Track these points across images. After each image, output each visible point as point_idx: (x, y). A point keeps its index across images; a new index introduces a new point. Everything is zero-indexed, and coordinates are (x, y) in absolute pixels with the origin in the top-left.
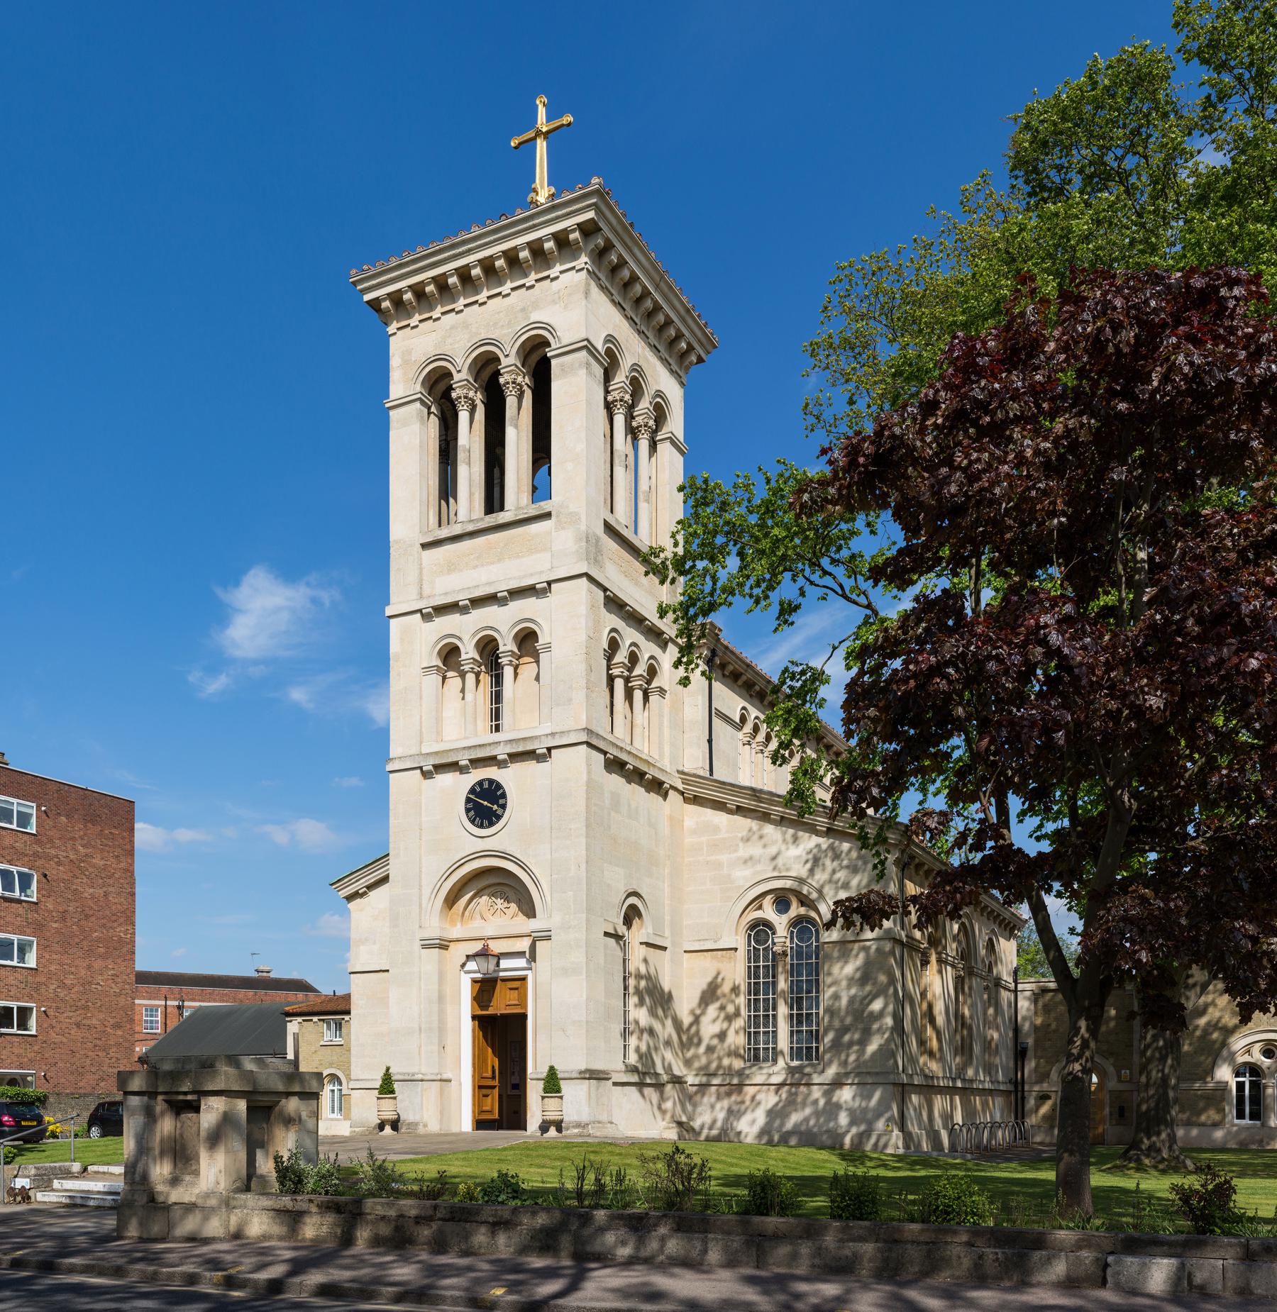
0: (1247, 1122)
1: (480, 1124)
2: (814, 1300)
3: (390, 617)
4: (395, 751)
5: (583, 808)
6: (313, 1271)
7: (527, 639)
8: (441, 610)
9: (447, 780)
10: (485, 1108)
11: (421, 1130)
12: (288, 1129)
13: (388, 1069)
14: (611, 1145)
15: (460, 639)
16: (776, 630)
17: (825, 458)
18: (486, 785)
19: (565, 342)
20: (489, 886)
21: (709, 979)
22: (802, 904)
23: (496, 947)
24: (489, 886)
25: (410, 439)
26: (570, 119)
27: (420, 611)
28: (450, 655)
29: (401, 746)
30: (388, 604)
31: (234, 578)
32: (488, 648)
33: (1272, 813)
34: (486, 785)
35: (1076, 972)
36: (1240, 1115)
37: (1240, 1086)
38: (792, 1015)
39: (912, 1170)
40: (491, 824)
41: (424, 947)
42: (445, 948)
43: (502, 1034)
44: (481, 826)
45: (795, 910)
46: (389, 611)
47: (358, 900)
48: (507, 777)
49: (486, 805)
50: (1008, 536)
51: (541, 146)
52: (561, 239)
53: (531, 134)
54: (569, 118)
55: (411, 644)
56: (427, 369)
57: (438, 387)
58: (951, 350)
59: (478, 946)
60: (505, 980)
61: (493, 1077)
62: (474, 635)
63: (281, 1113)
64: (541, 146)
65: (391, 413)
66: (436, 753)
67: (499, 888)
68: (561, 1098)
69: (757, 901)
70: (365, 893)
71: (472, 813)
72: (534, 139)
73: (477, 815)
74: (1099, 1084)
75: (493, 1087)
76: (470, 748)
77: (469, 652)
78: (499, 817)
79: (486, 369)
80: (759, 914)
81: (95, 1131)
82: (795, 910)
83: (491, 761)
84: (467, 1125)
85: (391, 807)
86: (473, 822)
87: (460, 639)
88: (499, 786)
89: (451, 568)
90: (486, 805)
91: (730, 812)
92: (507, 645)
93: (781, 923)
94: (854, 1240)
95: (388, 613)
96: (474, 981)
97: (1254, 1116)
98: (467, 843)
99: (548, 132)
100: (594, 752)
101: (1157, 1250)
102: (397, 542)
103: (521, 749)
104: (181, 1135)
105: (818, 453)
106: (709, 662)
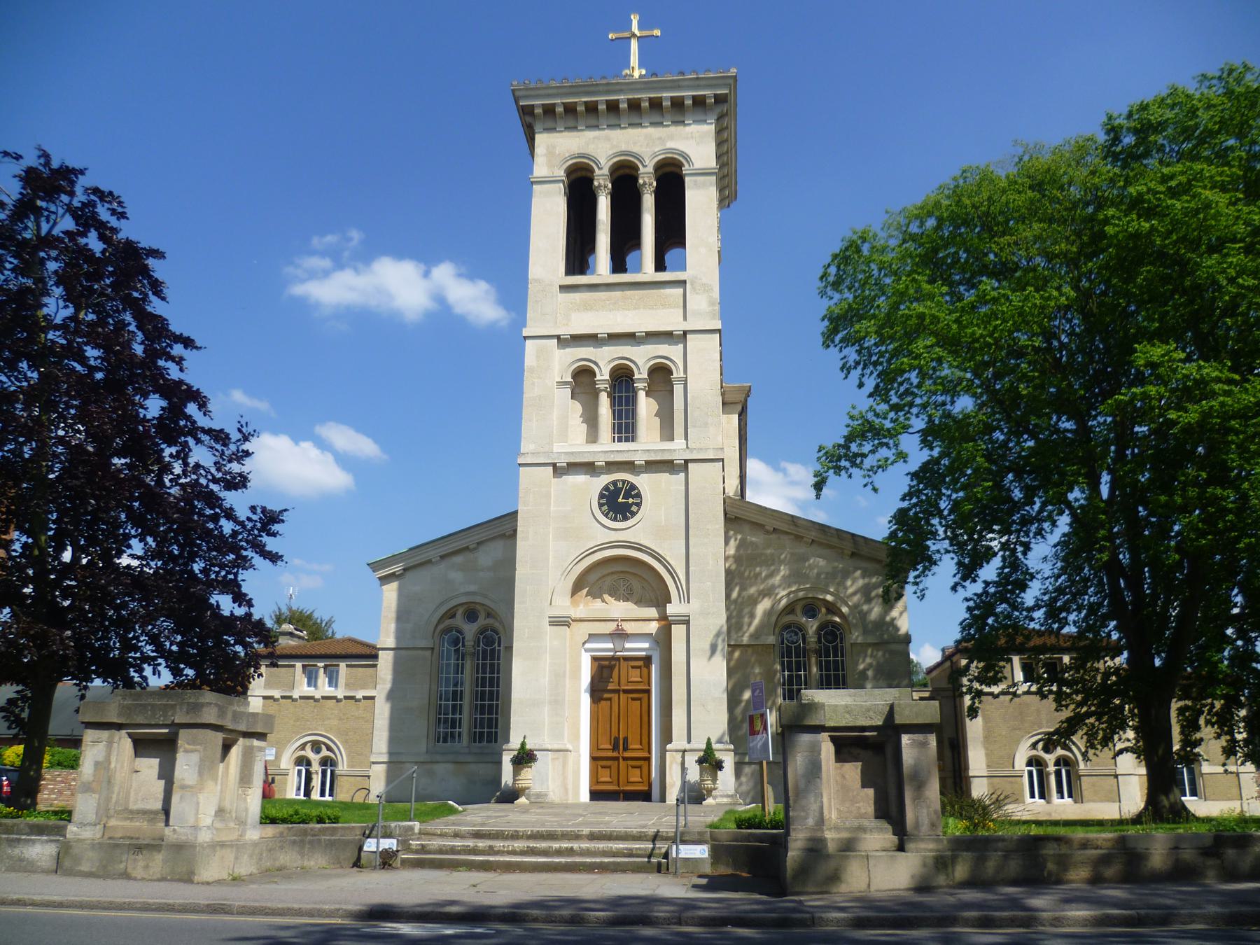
0: (1067, 800)
1: (596, 795)
3: (525, 338)
4: (524, 448)
6: (332, 424)
7: (661, 375)
8: (578, 340)
9: (581, 479)
10: (632, 779)
12: (894, 834)
13: (818, 497)
14: (1046, 159)
16: (15, 176)
18: (603, 501)
19: (696, 166)
22: (453, 616)
23: (629, 628)
25: (549, 215)
27: (558, 337)
28: (583, 377)
29: (529, 446)
32: (622, 378)
33: (4, 494)
35: (161, 363)
36: (1033, 796)
37: (1030, 773)
39: (801, 902)
40: (625, 519)
41: (552, 624)
45: (482, 621)
48: (643, 482)
49: (619, 503)
51: (634, 45)
52: (699, 102)
54: (657, 32)
57: (579, 187)
58: (977, 340)
59: (610, 628)
60: (626, 659)
62: (610, 362)
63: (201, 845)
64: (634, 45)
65: (751, 497)
66: (572, 453)
67: (622, 576)
68: (375, 666)
69: (451, 614)
70: (475, 549)
73: (610, 509)
76: (454, 866)
77: (603, 375)
78: (633, 514)
79: (625, 180)
80: (303, 753)
81: (268, 590)
83: (629, 466)
84: (585, 796)
86: (601, 505)
88: (601, 496)
89: (587, 307)
90: (619, 503)
91: (768, 532)
92: (641, 374)
93: (470, 630)
94: (334, 698)
95: (525, 334)
96: (594, 659)
97: (1042, 796)
98: (601, 534)
100: (195, 731)
101: (504, 914)
105: (814, 493)
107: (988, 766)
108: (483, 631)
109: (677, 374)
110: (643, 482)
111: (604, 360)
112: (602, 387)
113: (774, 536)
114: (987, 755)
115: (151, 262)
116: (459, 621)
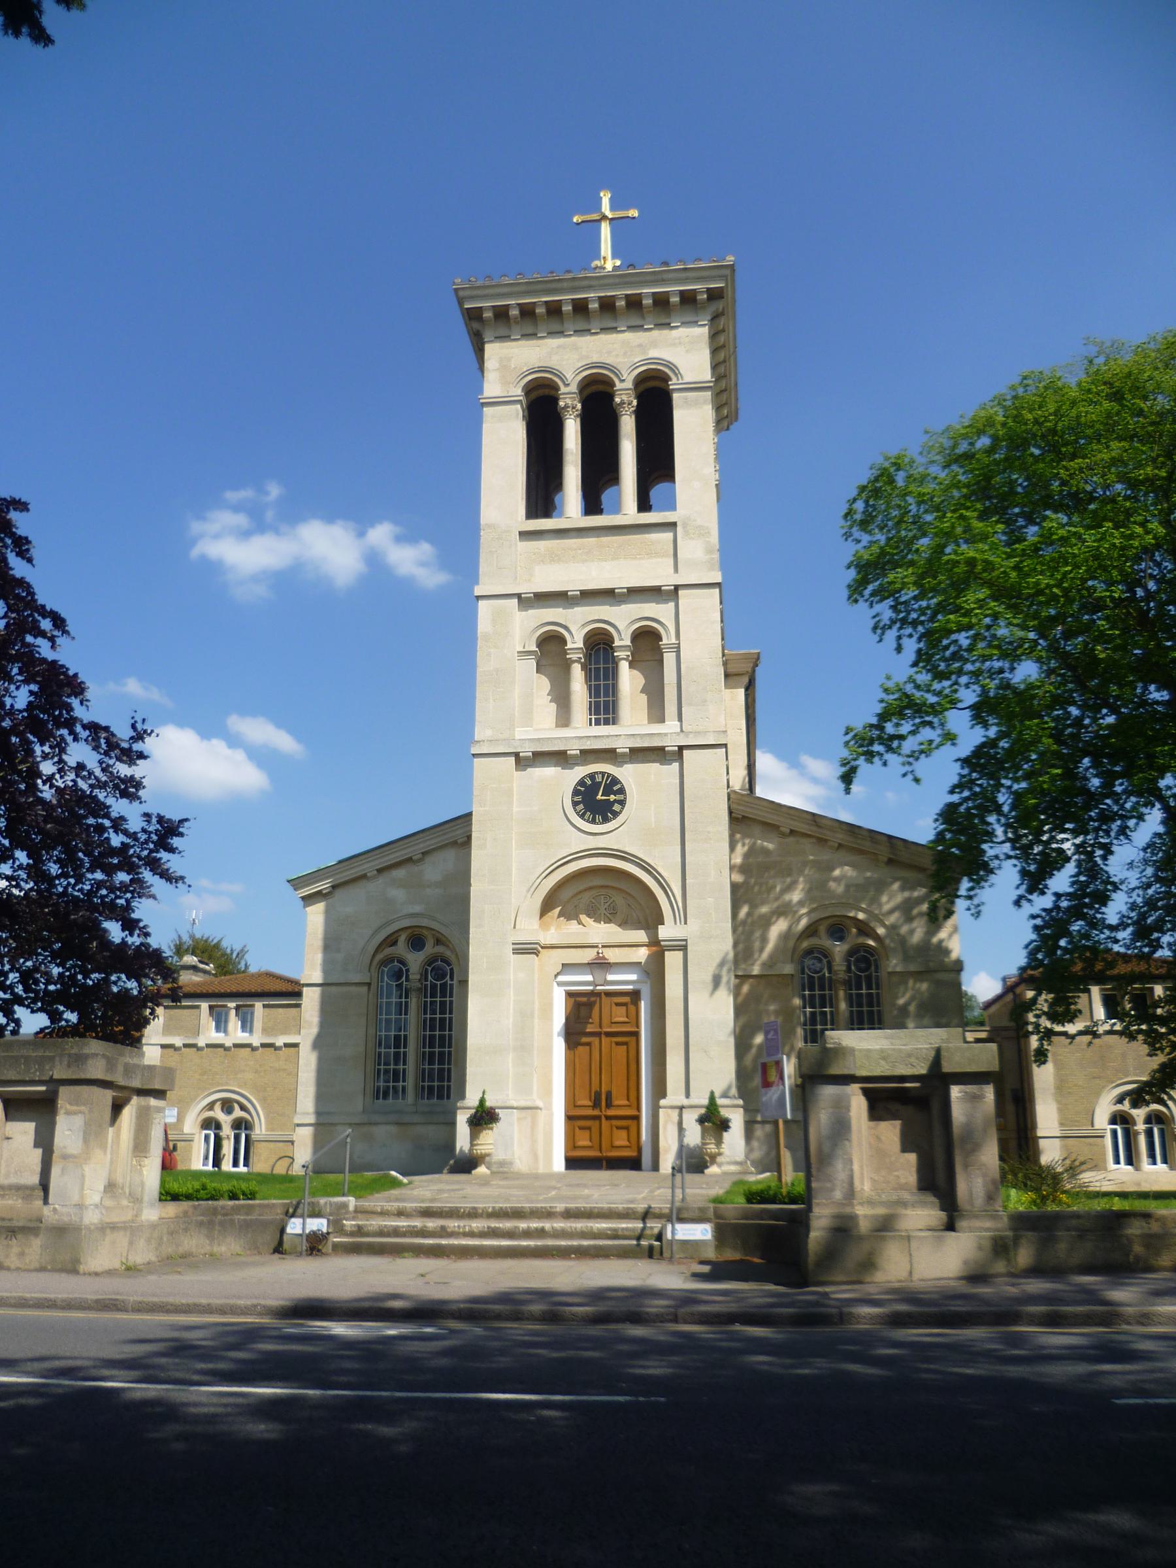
1: (573, 1163)
2: (756, 956)
5: (190, 1203)
7: (647, 640)
9: (549, 772)
11: (398, 530)
15: (566, 628)
17: (850, 539)
20: (591, 888)
21: (724, 792)
22: (395, 943)
23: (612, 956)
24: (591, 888)
25: (504, 443)
26: (636, 214)
28: (550, 645)
30: (477, 583)
31: (431, 541)
32: (599, 645)
34: (577, 799)
37: (1114, 1132)
38: (878, 1005)
40: (606, 820)
41: (517, 952)
42: (536, 953)
43: (541, 757)
44: (593, 822)
45: (430, 949)
46: (478, 591)
47: (655, 766)
48: (627, 774)
49: (598, 801)
50: (80, 977)
51: (605, 230)
52: (688, 299)
53: (595, 216)
54: (634, 213)
55: (505, 637)
56: (594, 371)
59: (588, 956)
60: (609, 994)
61: (589, 1128)
62: (633, 622)
64: (605, 230)
67: (603, 891)
68: (298, 1006)
69: (391, 941)
70: (420, 860)
71: (581, 806)
72: (599, 221)
73: (587, 809)
74: (958, 849)
75: (217, 1162)
77: (576, 642)
78: (616, 814)
80: (210, 1114)
82: (430, 949)
84: (559, 1164)
85: (476, 792)
87: (566, 628)
88: (576, 792)
89: (554, 558)
90: (598, 801)
91: (783, 835)
98: (575, 840)
99: (612, 219)
102: (489, 526)
103: (646, 744)
104: (894, 1238)
106: (938, 545)
107: (1061, 1124)
108: (431, 961)
109: (668, 639)
110: (627, 774)
111: (577, 624)
112: (574, 657)
113: (791, 839)
114: (1060, 1110)
115: (13, 515)
116: (401, 949)
